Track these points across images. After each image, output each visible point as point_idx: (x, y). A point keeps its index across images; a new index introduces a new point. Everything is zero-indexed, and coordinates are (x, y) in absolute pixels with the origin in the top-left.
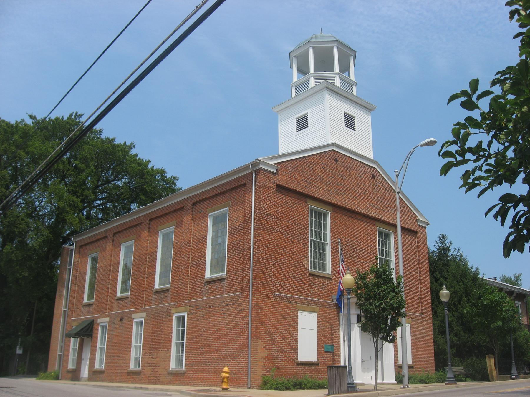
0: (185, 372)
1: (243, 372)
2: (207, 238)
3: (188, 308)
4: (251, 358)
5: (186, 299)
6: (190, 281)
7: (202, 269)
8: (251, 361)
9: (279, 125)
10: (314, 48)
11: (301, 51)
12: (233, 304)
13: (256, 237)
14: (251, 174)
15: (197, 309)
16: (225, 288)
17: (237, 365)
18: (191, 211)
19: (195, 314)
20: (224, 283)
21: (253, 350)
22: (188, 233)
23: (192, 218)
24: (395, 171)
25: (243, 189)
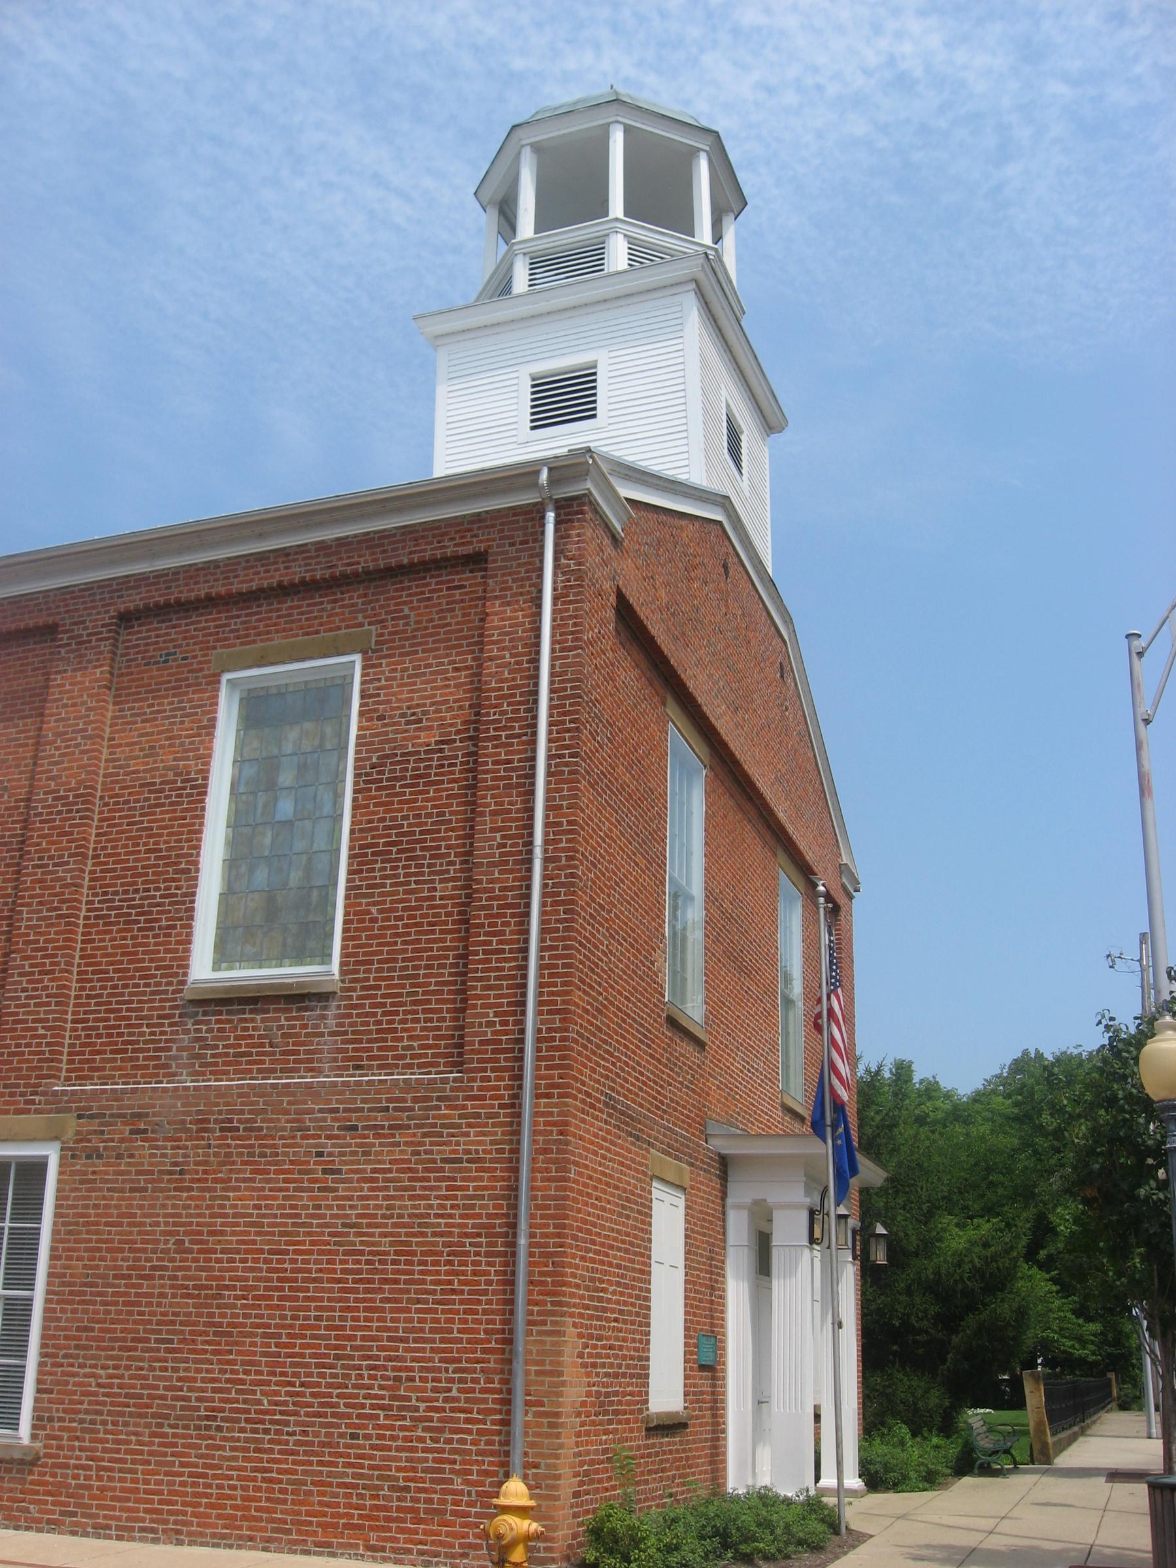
0: (34, 1462)
1: (467, 1482)
2: (206, 786)
3: (71, 1125)
4: (526, 1413)
5: (54, 1077)
6: (83, 989)
7: (169, 935)
8: (527, 1424)
9: (441, 391)
10: (628, 130)
11: (551, 135)
12: (391, 1127)
13: (560, 807)
14: (535, 514)
15: (132, 1132)
16: (327, 1044)
17: (421, 1440)
18: (105, 646)
19: (119, 1156)
20: (324, 1017)
21: (538, 1373)
22: (83, 752)
23: (111, 682)
24: (1128, 636)
25: (468, 578)
